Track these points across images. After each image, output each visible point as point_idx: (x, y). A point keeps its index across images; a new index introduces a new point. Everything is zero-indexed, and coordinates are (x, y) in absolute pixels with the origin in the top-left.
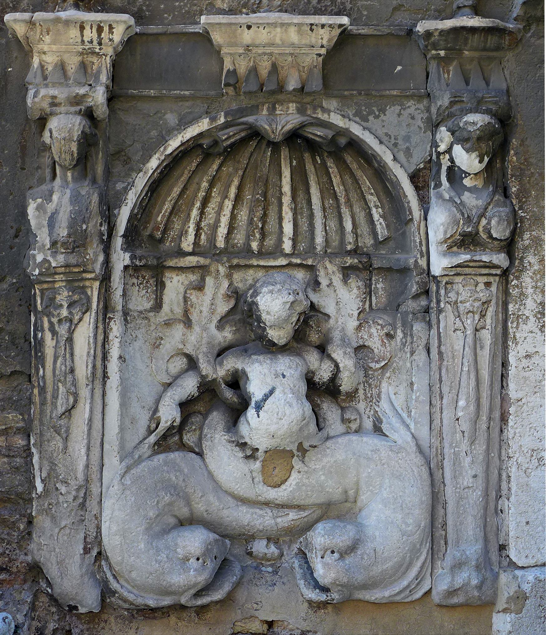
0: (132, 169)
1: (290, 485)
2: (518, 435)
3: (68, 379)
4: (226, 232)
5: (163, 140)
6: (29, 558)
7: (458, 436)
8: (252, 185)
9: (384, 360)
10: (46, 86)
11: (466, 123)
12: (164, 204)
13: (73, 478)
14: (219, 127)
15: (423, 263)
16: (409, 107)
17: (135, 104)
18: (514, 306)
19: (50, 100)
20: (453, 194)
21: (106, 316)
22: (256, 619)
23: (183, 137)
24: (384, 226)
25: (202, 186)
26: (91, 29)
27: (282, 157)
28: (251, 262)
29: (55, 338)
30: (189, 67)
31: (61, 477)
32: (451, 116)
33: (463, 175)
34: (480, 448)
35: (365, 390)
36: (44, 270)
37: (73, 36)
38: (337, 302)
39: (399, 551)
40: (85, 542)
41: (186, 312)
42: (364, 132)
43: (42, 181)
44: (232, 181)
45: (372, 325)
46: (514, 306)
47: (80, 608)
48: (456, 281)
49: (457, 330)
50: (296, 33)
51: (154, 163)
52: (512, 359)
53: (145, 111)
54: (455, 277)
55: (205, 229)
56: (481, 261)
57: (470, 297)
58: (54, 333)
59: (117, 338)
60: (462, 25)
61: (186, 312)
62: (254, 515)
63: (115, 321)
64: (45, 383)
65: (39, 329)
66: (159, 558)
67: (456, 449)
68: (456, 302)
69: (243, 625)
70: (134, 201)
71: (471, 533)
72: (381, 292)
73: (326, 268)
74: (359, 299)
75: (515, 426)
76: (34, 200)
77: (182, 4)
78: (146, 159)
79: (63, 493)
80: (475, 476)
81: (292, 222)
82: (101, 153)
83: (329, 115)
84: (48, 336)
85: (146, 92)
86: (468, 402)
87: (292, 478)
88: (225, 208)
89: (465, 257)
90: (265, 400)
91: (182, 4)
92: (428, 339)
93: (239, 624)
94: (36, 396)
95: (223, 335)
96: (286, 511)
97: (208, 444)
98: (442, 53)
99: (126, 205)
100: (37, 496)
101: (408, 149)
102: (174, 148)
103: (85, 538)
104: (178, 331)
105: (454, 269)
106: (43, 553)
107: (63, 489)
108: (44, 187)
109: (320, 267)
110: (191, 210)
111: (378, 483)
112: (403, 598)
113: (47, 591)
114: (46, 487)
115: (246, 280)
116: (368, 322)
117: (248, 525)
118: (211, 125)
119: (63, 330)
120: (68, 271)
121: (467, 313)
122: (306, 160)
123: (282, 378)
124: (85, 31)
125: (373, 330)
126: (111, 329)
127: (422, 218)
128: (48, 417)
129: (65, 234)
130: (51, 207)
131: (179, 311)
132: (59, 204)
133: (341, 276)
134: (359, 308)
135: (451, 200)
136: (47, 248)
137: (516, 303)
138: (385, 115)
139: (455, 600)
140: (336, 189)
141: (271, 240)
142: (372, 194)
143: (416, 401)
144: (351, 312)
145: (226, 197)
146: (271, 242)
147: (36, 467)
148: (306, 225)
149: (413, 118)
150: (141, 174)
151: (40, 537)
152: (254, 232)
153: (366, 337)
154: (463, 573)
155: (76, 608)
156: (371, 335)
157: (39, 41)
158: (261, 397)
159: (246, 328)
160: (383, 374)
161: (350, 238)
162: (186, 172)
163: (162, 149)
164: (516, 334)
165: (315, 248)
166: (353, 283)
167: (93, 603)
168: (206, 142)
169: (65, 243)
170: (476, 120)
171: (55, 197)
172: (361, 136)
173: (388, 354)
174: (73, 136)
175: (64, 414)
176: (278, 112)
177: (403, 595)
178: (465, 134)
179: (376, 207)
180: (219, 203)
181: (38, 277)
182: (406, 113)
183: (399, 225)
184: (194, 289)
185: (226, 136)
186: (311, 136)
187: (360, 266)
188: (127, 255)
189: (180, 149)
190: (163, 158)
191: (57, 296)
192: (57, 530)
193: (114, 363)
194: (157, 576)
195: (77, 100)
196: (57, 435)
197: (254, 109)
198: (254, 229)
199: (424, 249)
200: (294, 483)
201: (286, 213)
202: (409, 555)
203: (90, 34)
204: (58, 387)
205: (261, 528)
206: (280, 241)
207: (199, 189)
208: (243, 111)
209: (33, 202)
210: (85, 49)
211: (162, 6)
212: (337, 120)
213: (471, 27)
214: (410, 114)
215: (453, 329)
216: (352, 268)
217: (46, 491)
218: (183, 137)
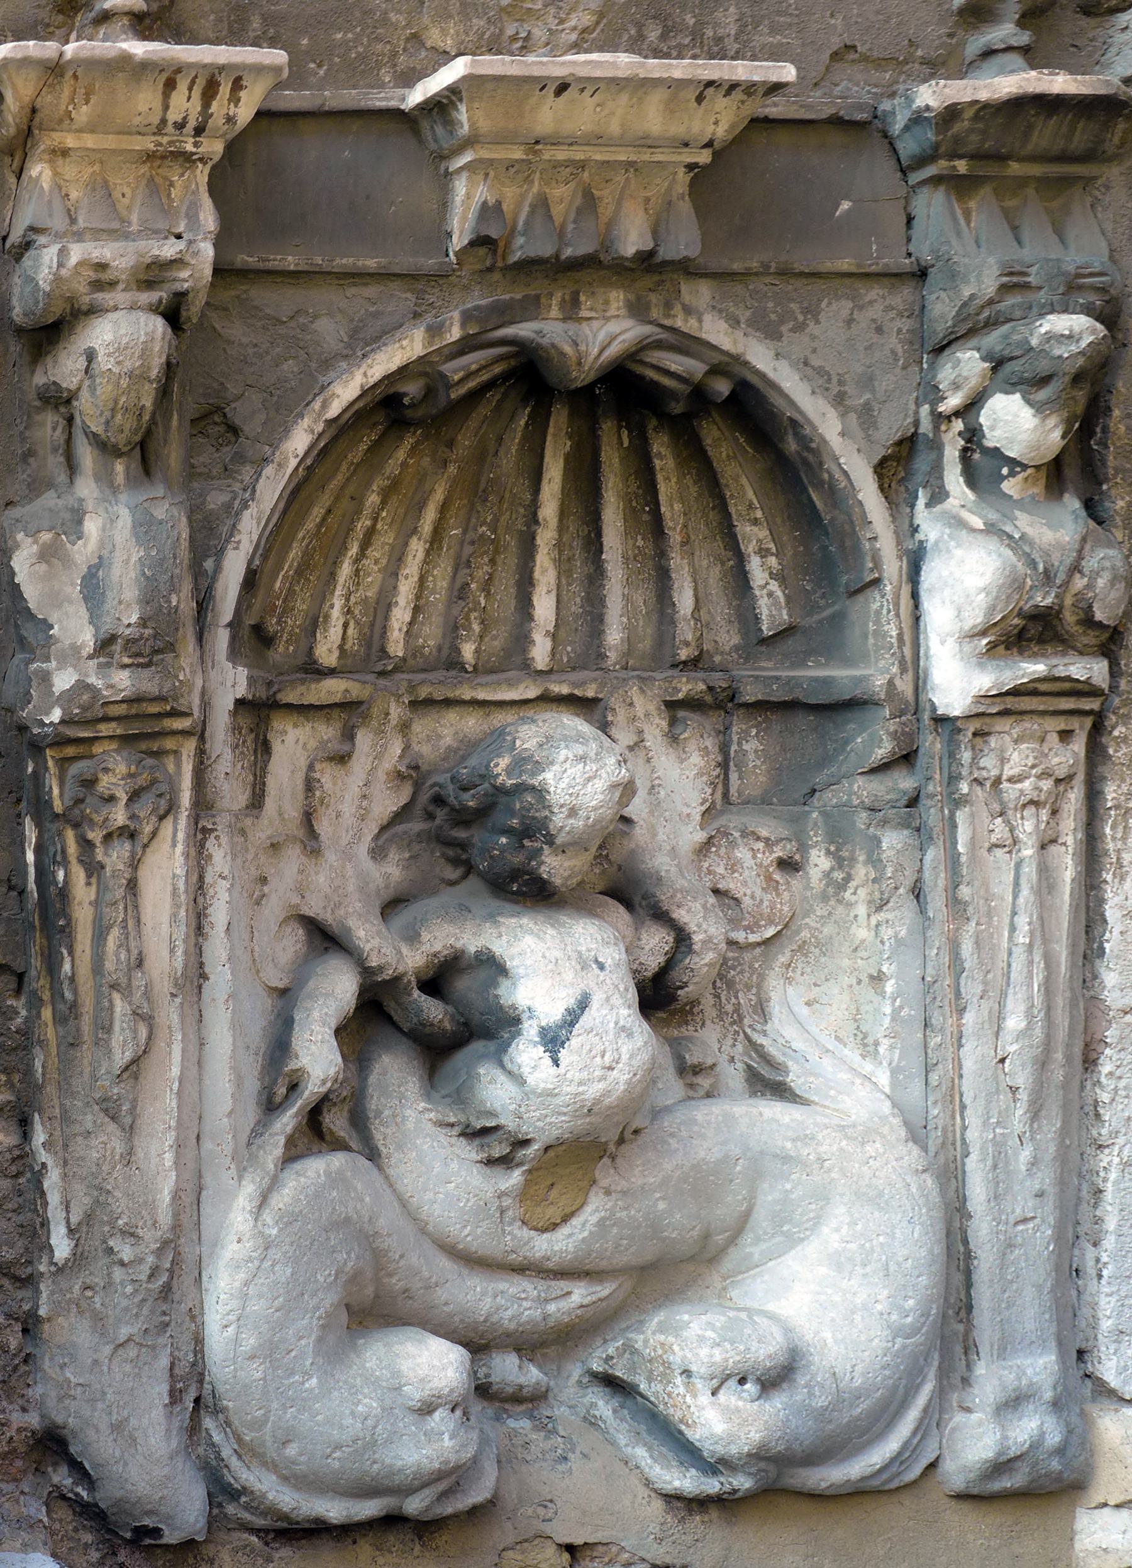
0: (240, 458)
1: (584, 1225)
2: (1122, 1093)
3: (135, 983)
4: (408, 618)
5: (311, 387)
6: (33, 1420)
7: (1004, 1098)
8: (465, 501)
9: (771, 922)
10: (79, 236)
11: (1050, 337)
12: (290, 546)
13: (149, 1223)
14: (446, 351)
15: (904, 686)
16: (871, 302)
17: (245, 291)
18: (1119, 786)
19: (91, 273)
20: (993, 516)
21: (196, 824)
22: (549, 1543)
23: (365, 374)
24: (782, 600)
25: (368, 504)
26: (190, 89)
27: (551, 430)
28: (457, 693)
29: (94, 880)
30: (368, 197)
31: (120, 1222)
32: (991, 324)
33: (1005, 471)
34: (1051, 1126)
35: (717, 996)
36: (77, 711)
37: (142, 107)
38: (653, 787)
39: (887, 1372)
40: (171, 1376)
41: (308, 818)
42: (777, 363)
43: (38, 486)
44: (432, 490)
45: (739, 841)
46: (1119, 786)
47: (167, 1533)
48: (998, 728)
49: (997, 846)
50: (661, 107)
51: (299, 441)
52: (1112, 913)
53: (268, 311)
54: (998, 720)
55: (357, 612)
56: (1068, 679)
57: (1033, 767)
58: (94, 869)
59: (224, 878)
60: (1038, 90)
61: (308, 818)
62: (499, 1299)
63: (217, 838)
64: (75, 992)
65: (59, 858)
66: (360, 1408)
67: (998, 1131)
68: (998, 781)
69: (519, 1558)
70: (255, 537)
71: (1030, 1326)
72: (752, 761)
73: (631, 704)
74: (705, 778)
75: (1118, 1073)
76: (34, 534)
77: (350, 35)
78: (278, 431)
79: (126, 1259)
80: (1040, 1195)
81: (554, 593)
82: (175, 417)
83: (700, 321)
84: (79, 874)
85: (276, 261)
86: (1030, 1016)
87: (588, 1209)
88: (410, 557)
89: (1034, 668)
90: (572, 1024)
91: (350, 35)
92: (920, 871)
93: (510, 1554)
94: (46, 1025)
95: (383, 870)
96: (563, 1285)
97: (389, 1131)
98: (962, 166)
99: (236, 548)
100: (53, 1269)
101: (867, 409)
102: (345, 404)
103: (172, 1365)
104: (292, 860)
105: (998, 700)
106: (73, 1405)
107: (126, 1252)
108: (49, 499)
109: (614, 702)
110: (336, 564)
111: (812, 1215)
112: (883, 1484)
113: (77, 1494)
114: (80, 1249)
115: (440, 737)
116: (727, 834)
117: (485, 1321)
118: (431, 344)
119: (115, 857)
120: (134, 711)
121: (1024, 806)
122: (605, 439)
123: (597, 971)
124: (174, 94)
125: (742, 853)
126: (210, 856)
127: (904, 577)
128: (86, 1076)
129: (134, 619)
130: (84, 551)
131: (293, 813)
132: (106, 541)
133: (664, 724)
134: (704, 801)
135: (991, 529)
136: (84, 653)
137: (1123, 780)
138: (818, 322)
139: (1006, 1483)
140: (663, 509)
141: (495, 638)
142: (755, 522)
143: (893, 1019)
144: (686, 811)
145: (414, 531)
146: (496, 643)
147: (54, 1198)
148: (578, 600)
149: (879, 330)
150: (269, 470)
151: (63, 1366)
152: (467, 618)
153: (721, 870)
154: (1025, 1419)
155: (156, 1532)
156: (733, 865)
157: (61, 121)
158: (559, 1017)
159: (432, 852)
160: (767, 959)
161: (686, 631)
162: (344, 467)
163: (317, 405)
164: (1124, 855)
165: (602, 656)
166: (693, 741)
167: (197, 1521)
168: (412, 389)
169: (135, 641)
170: (1077, 329)
171: (92, 526)
172: (771, 375)
173: (786, 908)
174: (149, 368)
175: (127, 1068)
176: (584, 313)
177: (885, 1476)
178: (1043, 367)
179: (763, 553)
180: (393, 547)
181: (61, 729)
182: (864, 318)
183: (823, 596)
184: (331, 759)
185: (461, 374)
186: (651, 374)
187: (709, 699)
188: (242, 673)
189: (356, 407)
190: (320, 427)
191: (100, 775)
192: (107, 1350)
193: (218, 941)
194: (356, 1451)
195: (152, 275)
196: (107, 1119)
197: (531, 308)
198: (470, 610)
199: (907, 651)
200: (594, 1219)
201: (544, 571)
202: (904, 1382)
203: (184, 104)
204: (111, 1001)
205: (513, 1326)
206: (522, 640)
207: (358, 512)
208: (506, 313)
209: (30, 540)
210: (160, 144)
211: (305, 42)
212: (716, 332)
213: (1058, 95)
214: (874, 320)
215: (987, 845)
216: (692, 704)
217: (78, 1258)
218: (365, 374)
